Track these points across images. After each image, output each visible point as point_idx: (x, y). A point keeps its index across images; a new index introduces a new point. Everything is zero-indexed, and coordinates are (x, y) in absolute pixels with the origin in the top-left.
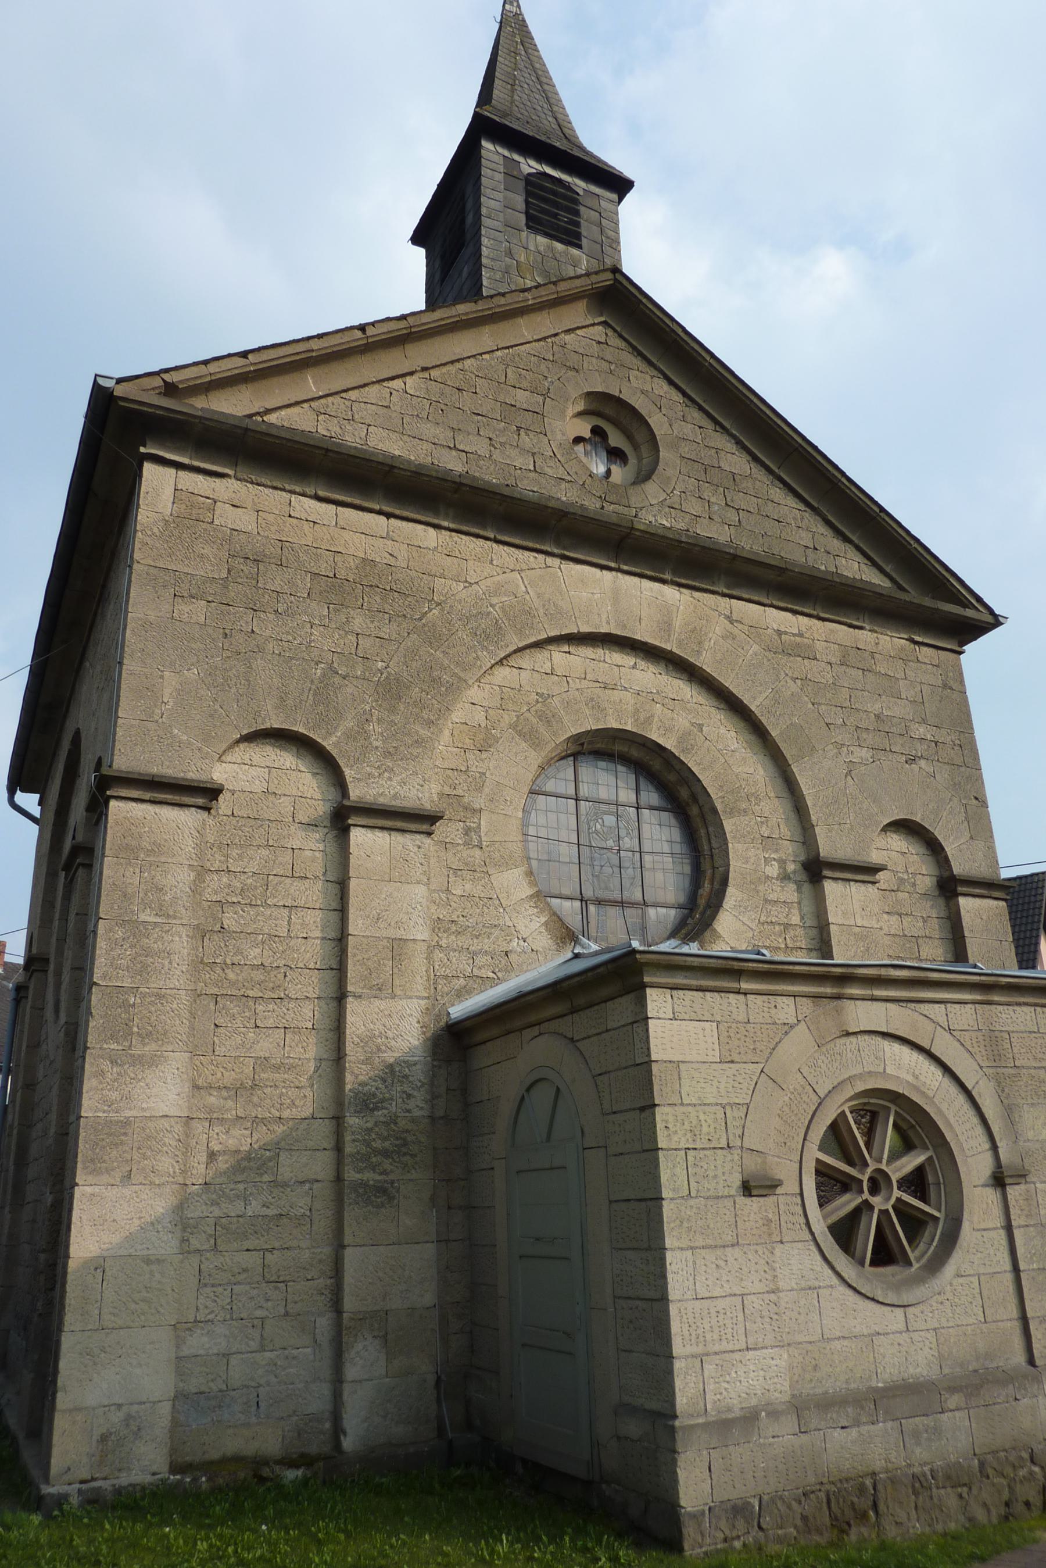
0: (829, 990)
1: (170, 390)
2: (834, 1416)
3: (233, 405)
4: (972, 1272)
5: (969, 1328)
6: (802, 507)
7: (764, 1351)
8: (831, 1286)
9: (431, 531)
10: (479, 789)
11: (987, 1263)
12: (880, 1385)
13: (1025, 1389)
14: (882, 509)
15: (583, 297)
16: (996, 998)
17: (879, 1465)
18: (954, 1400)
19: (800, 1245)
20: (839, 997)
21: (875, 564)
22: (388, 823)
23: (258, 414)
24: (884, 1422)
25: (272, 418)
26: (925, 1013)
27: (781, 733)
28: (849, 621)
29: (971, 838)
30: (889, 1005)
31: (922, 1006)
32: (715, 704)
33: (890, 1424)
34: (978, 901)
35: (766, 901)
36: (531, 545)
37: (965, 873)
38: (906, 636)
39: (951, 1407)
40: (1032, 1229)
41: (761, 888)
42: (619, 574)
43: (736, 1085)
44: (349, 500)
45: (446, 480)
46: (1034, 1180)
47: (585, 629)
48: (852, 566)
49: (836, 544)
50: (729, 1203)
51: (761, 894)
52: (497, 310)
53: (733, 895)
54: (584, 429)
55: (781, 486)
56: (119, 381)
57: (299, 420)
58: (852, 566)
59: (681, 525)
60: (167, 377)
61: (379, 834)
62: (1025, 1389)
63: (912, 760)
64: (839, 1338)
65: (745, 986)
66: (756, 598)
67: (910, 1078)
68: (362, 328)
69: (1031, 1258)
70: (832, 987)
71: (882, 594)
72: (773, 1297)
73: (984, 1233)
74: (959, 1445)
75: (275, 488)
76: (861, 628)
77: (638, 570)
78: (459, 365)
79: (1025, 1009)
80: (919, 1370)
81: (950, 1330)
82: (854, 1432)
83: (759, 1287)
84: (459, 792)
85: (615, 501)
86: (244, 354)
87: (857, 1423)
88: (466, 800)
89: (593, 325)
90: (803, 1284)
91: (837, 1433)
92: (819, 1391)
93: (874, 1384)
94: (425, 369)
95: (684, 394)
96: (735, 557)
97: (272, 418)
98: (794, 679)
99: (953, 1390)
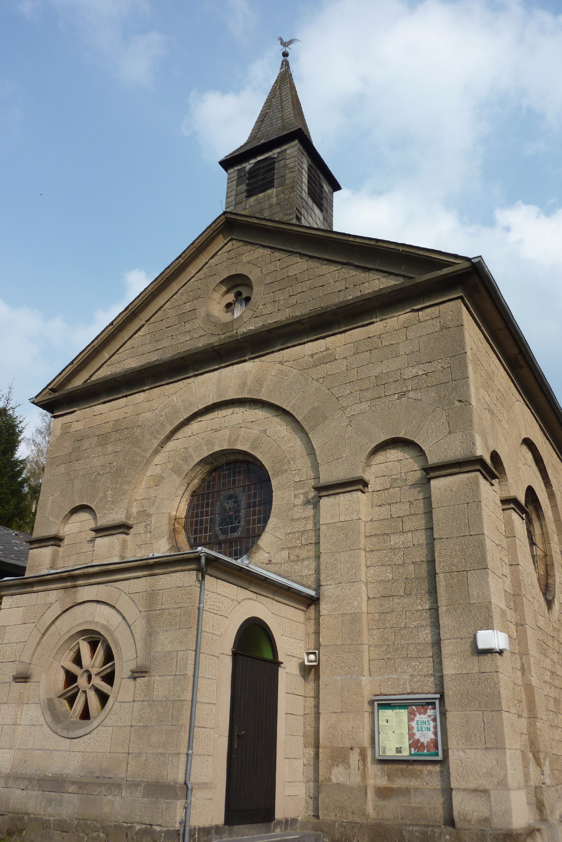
0: (69, 584)
1: (53, 390)
2: (19, 783)
3: (78, 382)
4: (110, 725)
5: (100, 754)
6: (339, 267)
7: (5, 750)
8: (42, 725)
9: (142, 394)
10: (153, 504)
11: (119, 720)
12: (50, 775)
13: (111, 790)
14: (377, 240)
15: (217, 235)
16: (157, 571)
17: (30, 810)
18: (72, 788)
19: (34, 705)
20: (75, 587)
21: (390, 274)
22: (104, 534)
23: (88, 379)
24: (38, 791)
25: (93, 378)
26: (117, 587)
27: (304, 418)
28: (360, 324)
29: (450, 432)
30: (100, 586)
31: (117, 583)
32: (275, 414)
33: (40, 792)
34: (450, 478)
35: (292, 520)
36: (180, 378)
37: (441, 461)
38: (409, 310)
39: (70, 791)
40: (146, 703)
41: (290, 513)
42: (222, 370)
43: (24, 633)
44: (446, 299)
45: (134, 372)
46: (154, 674)
47: (201, 407)
48: (376, 283)
49: (363, 276)
50: (8, 685)
51: (290, 517)
52: (167, 276)
53: (272, 521)
54: (230, 297)
55: (327, 262)
56: (36, 397)
57: (105, 372)
58: (376, 283)
59: (260, 324)
60: (50, 387)
61: (105, 538)
62: (111, 790)
63: (403, 394)
64: (39, 749)
65: (35, 589)
66: (297, 343)
67: (105, 623)
68: (111, 324)
69: (140, 719)
70: (71, 582)
71: (369, 299)
72: (14, 727)
73: (122, 704)
74: (69, 811)
75: (90, 407)
76: (372, 323)
77: (229, 363)
78: (163, 309)
79: (177, 574)
80: (69, 771)
81: (91, 754)
82: (25, 792)
83: (9, 722)
84: (145, 509)
85: (226, 331)
86: (72, 363)
87: (27, 789)
88: (147, 511)
89: (226, 244)
90: (31, 723)
91: (18, 792)
92: (24, 772)
93: (47, 774)
94: (147, 321)
95: (271, 248)
96: (269, 331)
97: (93, 378)
98: (317, 380)
99: (73, 783)
